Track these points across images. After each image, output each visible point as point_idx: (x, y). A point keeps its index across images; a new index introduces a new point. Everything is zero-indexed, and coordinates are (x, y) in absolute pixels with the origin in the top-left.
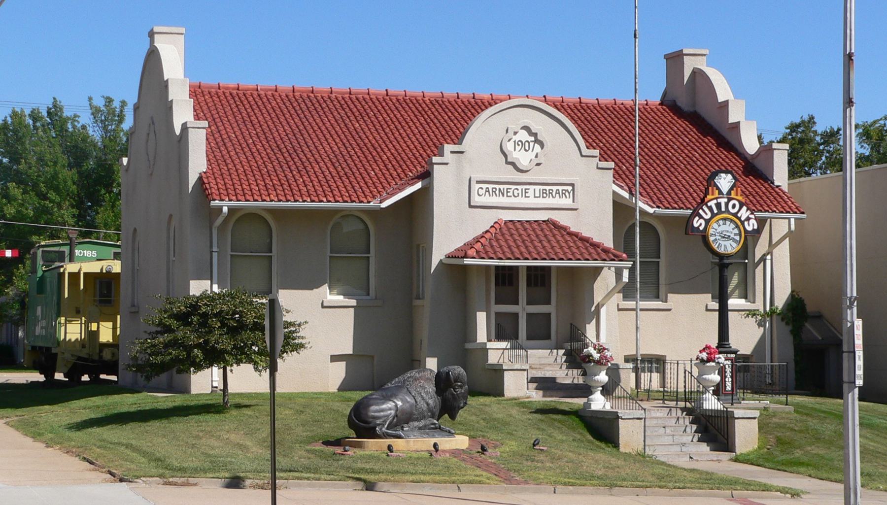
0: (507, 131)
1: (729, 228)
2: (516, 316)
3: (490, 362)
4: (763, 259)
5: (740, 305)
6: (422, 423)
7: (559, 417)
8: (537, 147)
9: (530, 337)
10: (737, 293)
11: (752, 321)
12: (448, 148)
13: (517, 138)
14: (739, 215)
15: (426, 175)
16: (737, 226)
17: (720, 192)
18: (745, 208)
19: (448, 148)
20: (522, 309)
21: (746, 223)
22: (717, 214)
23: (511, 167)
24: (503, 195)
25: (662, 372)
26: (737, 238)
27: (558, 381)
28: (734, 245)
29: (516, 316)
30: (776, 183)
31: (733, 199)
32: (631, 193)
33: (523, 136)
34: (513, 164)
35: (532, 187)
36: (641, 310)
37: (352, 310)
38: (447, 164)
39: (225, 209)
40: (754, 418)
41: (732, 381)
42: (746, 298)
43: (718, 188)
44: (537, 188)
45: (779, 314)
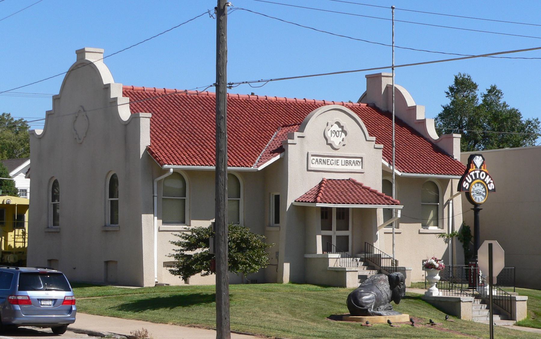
0: (327, 125)
1: (480, 188)
3: (330, 266)
4: (448, 203)
5: (436, 230)
6: (386, 306)
7: (412, 300)
8: (343, 134)
10: (432, 223)
11: (442, 240)
12: (296, 134)
13: (332, 129)
15: (282, 150)
16: (484, 187)
17: (476, 167)
18: (488, 176)
19: (296, 134)
22: (475, 180)
23: (329, 146)
26: (484, 194)
28: (483, 198)
31: (483, 171)
32: (390, 163)
33: (336, 128)
34: (331, 145)
36: (396, 233)
38: (295, 144)
39: (172, 170)
40: (525, 301)
43: (475, 165)
45: (457, 236)
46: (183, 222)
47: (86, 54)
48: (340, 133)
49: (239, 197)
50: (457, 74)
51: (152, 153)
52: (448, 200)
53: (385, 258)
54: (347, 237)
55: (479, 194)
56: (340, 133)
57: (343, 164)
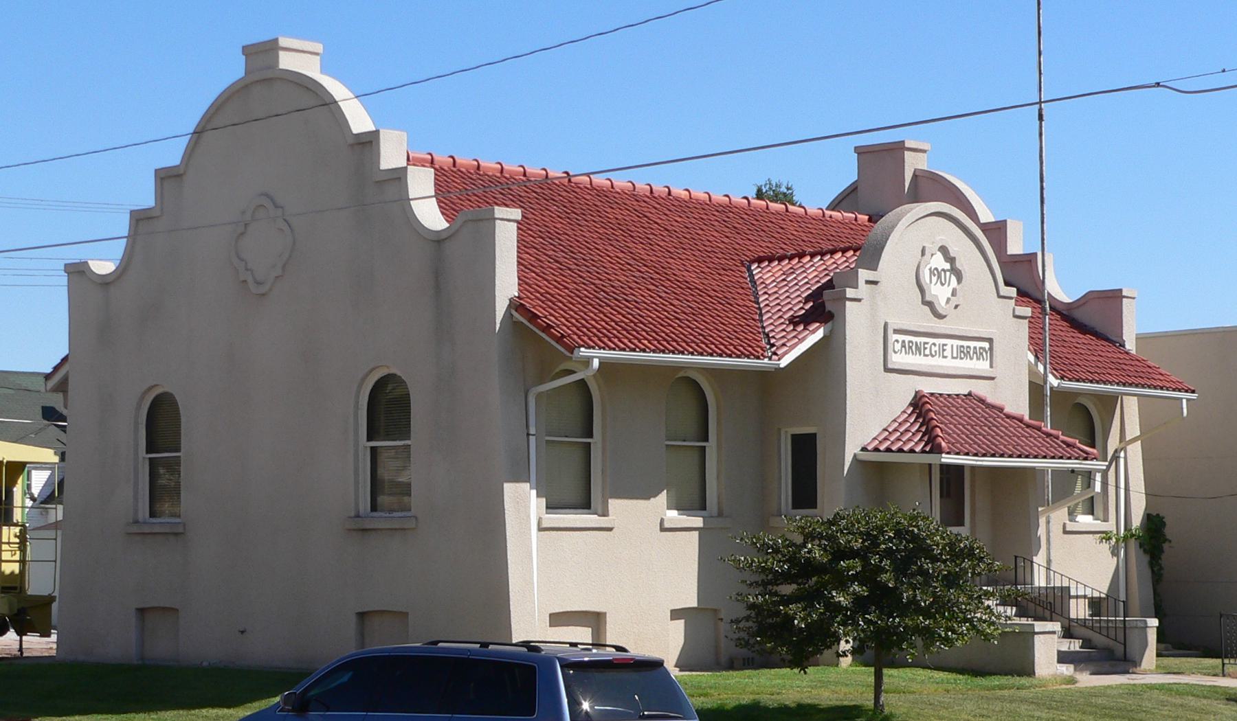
0: (923, 253)
4: (1116, 457)
8: (954, 278)
11: (1105, 547)
12: (864, 274)
15: (822, 308)
19: (864, 274)
23: (927, 309)
32: (1036, 356)
33: (939, 262)
34: (930, 304)
37: (696, 534)
39: (596, 363)
42: (1092, 514)
46: (585, 505)
47: (281, 53)
49: (706, 439)
50: (761, 182)
51: (533, 317)
52: (1116, 451)
53: (1077, 597)
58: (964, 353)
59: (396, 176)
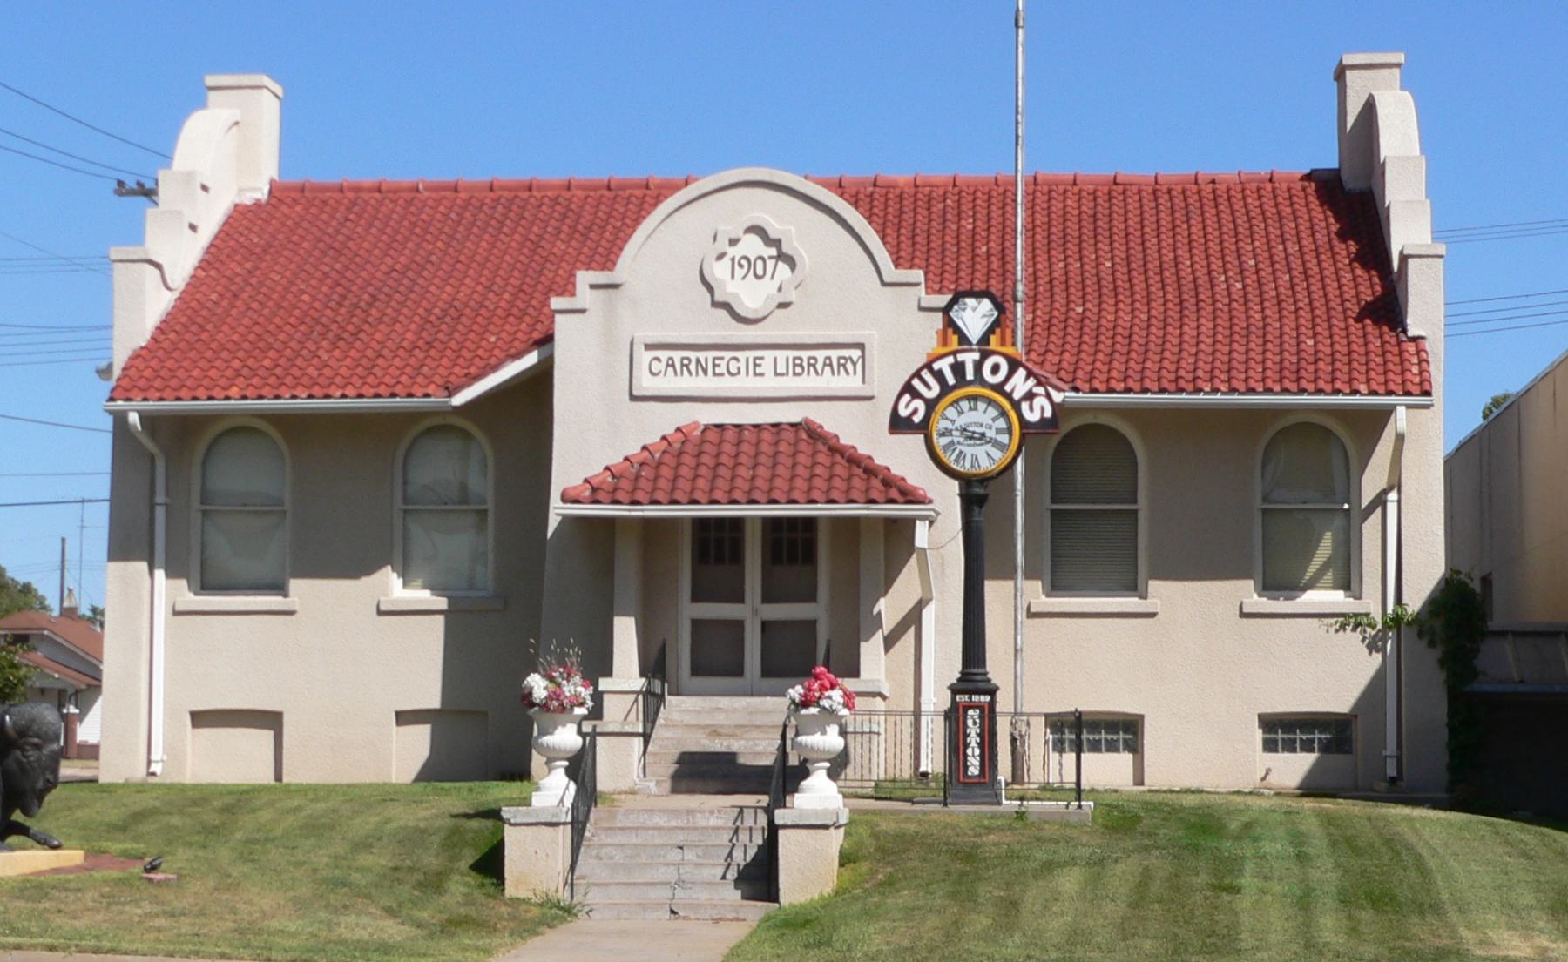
0: (715, 238)
2: (738, 625)
4: (1380, 501)
8: (783, 267)
9: (696, 671)
11: (1353, 639)
12: (584, 278)
14: (1008, 388)
15: (547, 340)
17: (963, 339)
19: (584, 278)
20: (752, 612)
21: (1025, 406)
22: (954, 387)
23: (723, 313)
24: (705, 372)
25: (1135, 747)
27: (741, 760)
28: (997, 454)
29: (738, 625)
30: (1412, 332)
33: (752, 246)
34: (726, 306)
35: (768, 355)
37: (441, 619)
38: (583, 311)
41: (982, 755)
44: (782, 355)
48: (770, 264)
54: (810, 626)
55: (975, 437)
56: (770, 264)
57: (782, 369)
58: (798, 367)
59: (1041, 199)
